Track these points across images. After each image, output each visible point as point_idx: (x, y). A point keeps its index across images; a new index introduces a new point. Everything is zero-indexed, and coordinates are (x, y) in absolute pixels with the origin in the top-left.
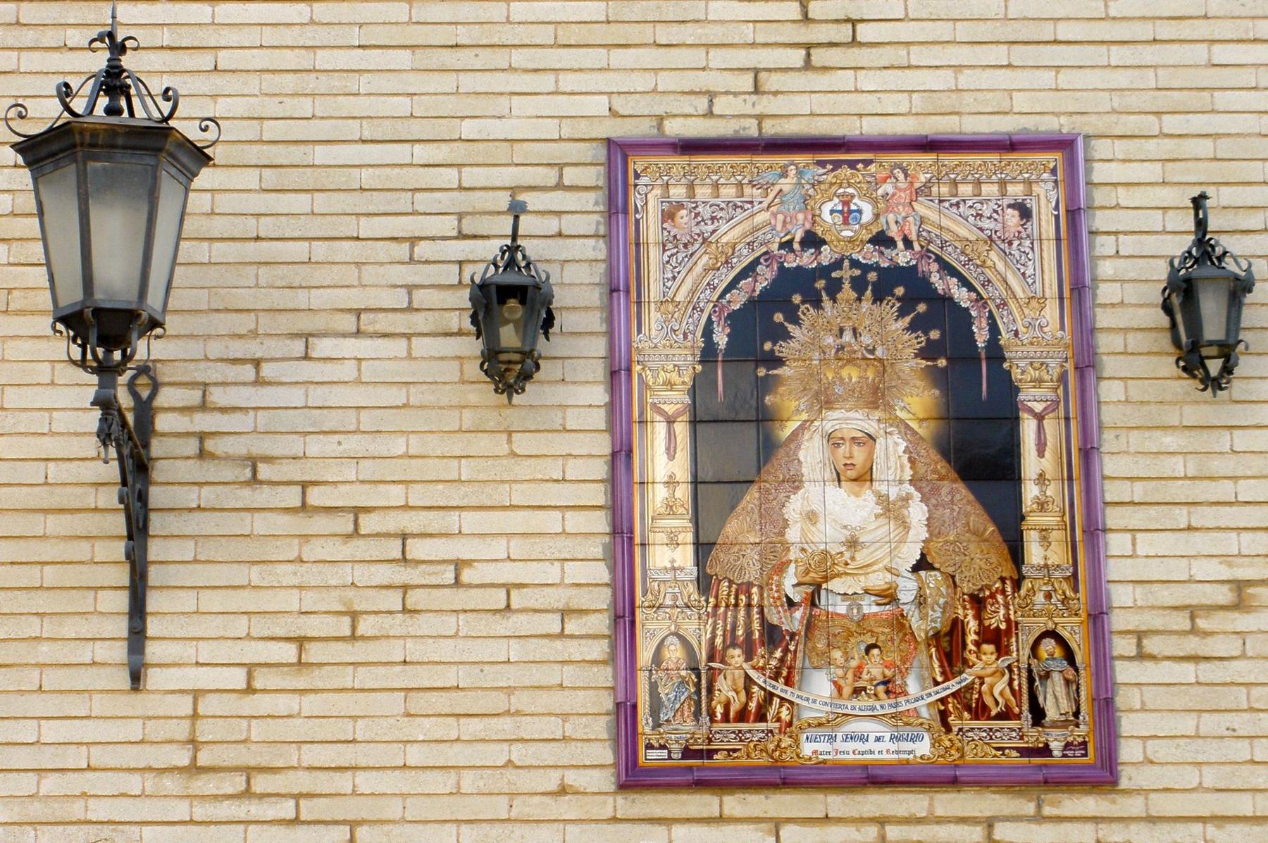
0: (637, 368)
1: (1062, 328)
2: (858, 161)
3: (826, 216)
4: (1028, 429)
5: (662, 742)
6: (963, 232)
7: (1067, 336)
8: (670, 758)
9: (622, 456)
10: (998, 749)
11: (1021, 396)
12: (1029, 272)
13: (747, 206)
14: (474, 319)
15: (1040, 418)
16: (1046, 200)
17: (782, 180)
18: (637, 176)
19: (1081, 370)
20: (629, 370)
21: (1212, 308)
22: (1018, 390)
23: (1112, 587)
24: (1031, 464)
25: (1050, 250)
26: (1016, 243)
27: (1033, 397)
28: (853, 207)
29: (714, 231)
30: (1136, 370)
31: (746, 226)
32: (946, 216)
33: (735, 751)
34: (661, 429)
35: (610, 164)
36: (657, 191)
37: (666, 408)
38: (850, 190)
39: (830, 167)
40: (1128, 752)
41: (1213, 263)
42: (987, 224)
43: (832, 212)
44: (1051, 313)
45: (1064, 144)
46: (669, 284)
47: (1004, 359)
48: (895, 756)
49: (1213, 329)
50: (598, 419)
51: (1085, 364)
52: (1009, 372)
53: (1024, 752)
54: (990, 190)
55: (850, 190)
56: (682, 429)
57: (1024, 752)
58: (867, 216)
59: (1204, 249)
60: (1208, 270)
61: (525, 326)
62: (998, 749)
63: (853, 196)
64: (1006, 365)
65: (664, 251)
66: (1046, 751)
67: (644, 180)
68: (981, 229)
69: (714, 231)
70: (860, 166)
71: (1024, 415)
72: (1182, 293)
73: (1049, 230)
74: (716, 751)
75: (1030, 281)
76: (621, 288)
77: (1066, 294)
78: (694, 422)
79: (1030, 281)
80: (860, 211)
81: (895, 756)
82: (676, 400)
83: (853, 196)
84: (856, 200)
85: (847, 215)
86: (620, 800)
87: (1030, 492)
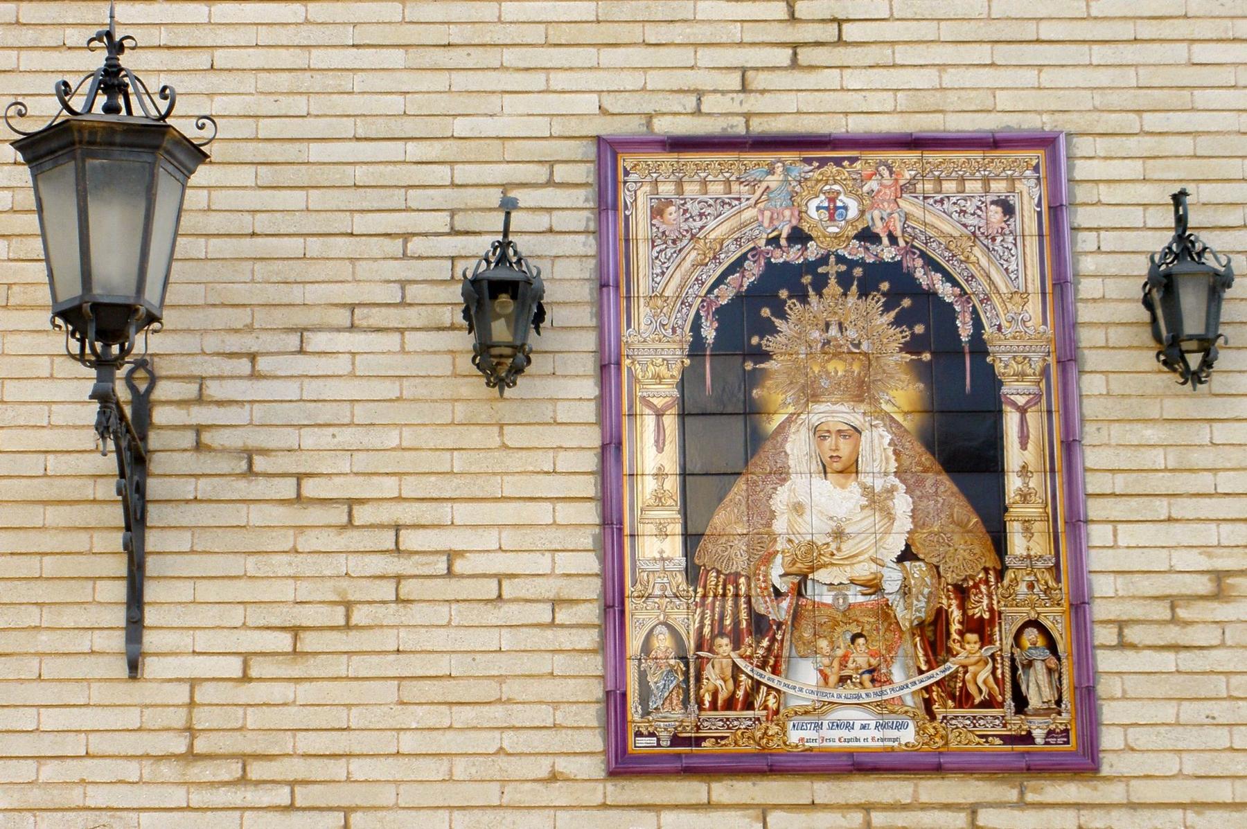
0: (626, 362)
1: (1045, 322)
2: (844, 159)
3: (813, 212)
4: (1011, 422)
5: (651, 730)
6: (947, 228)
7: (1049, 331)
8: (659, 745)
9: (612, 448)
10: (981, 736)
11: (1004, 390)
12: (1012, 267)
13: (735, 202)
14: (467, 314)
15: (1023, 411)
16: (1028, 196)
17: (770, 177)
18: (627, 173)
19: (1063, 364)
20: (619, 364)
21: (1192, 303)
22: (1001, 383)
23: (1094, 577)
24: (1014, 456)
25: (1032, 245)
26: (999, 239)
27: (1015, 390)
28: (839, 204)
29: (702, 228)
30: (1117, 364)
31: (734, 222)
32: (930, 213)
33: (723, 738)
34: (650, 421)
35: (599, 161)
36: (647, 188)
37: (655, 401)
38: (836, 187)
39: (816, 164)
40: (1109, 739)
41: (1193, 259)
42: (971, 220)
43: (818, 208)
44: (1033, 308)
45: (1046, 142)
46: (658, 279)
47: (987, 353)
48: (881, 744)
49: (1193, 324)
50: (588, 412)
51: (1067, 358)
52: (992, 366)
53: (1007, 739)
54: (973, 186)
55: (836, 187)
56: (671, 422)
57: (1007, 739)
58: (853, 213)
59: (1184, 245)
60: (1188, 266)
61: (517, 321)
62: (981, 736)
63: (838, 193)
64: (989, 359)
65: (653, 246)
66: (1028, 738)
67: (633, 177)
68: (965, 226)
69: (702, 228)
70: (846, 163)
71: (1007, 408)
72: (1162, 288)
73: (1031, 226)
74: (704, 739)
75: (1013, 276)
76: (611, 283)
77: (1049, 289)
78: (683, 415)
79: (1013, 276)
80: (845, 208)
81: (881, 744)
82: (665, 393)
83: (838, 193)
84: (842, 197)
85: (833, 211)
86: (610, 786)
87: (1013, 484)
